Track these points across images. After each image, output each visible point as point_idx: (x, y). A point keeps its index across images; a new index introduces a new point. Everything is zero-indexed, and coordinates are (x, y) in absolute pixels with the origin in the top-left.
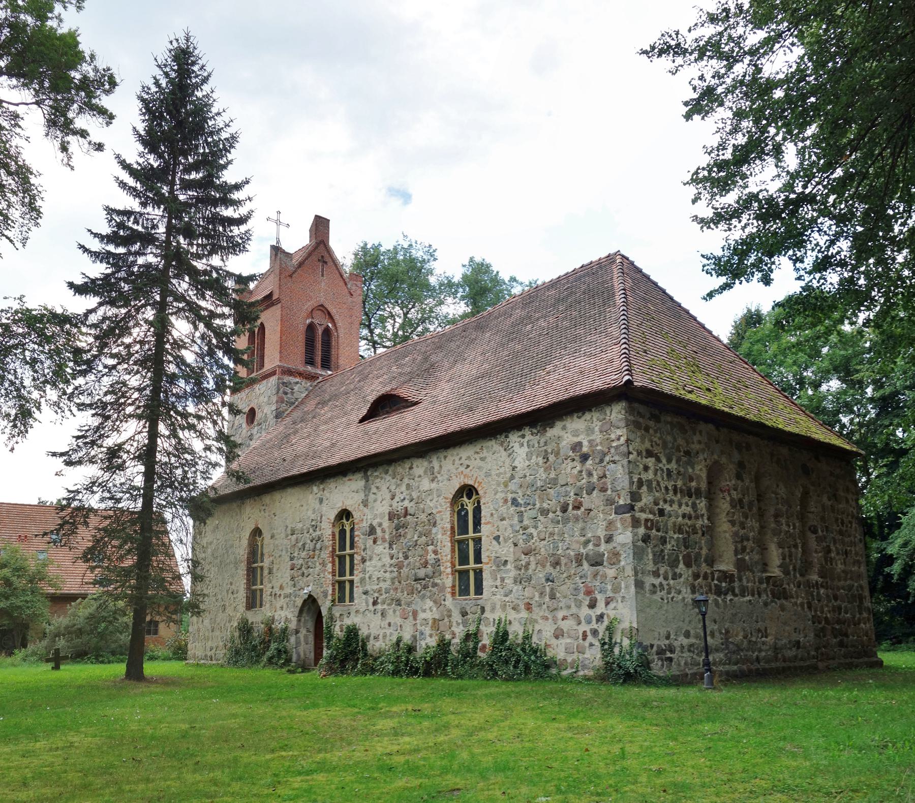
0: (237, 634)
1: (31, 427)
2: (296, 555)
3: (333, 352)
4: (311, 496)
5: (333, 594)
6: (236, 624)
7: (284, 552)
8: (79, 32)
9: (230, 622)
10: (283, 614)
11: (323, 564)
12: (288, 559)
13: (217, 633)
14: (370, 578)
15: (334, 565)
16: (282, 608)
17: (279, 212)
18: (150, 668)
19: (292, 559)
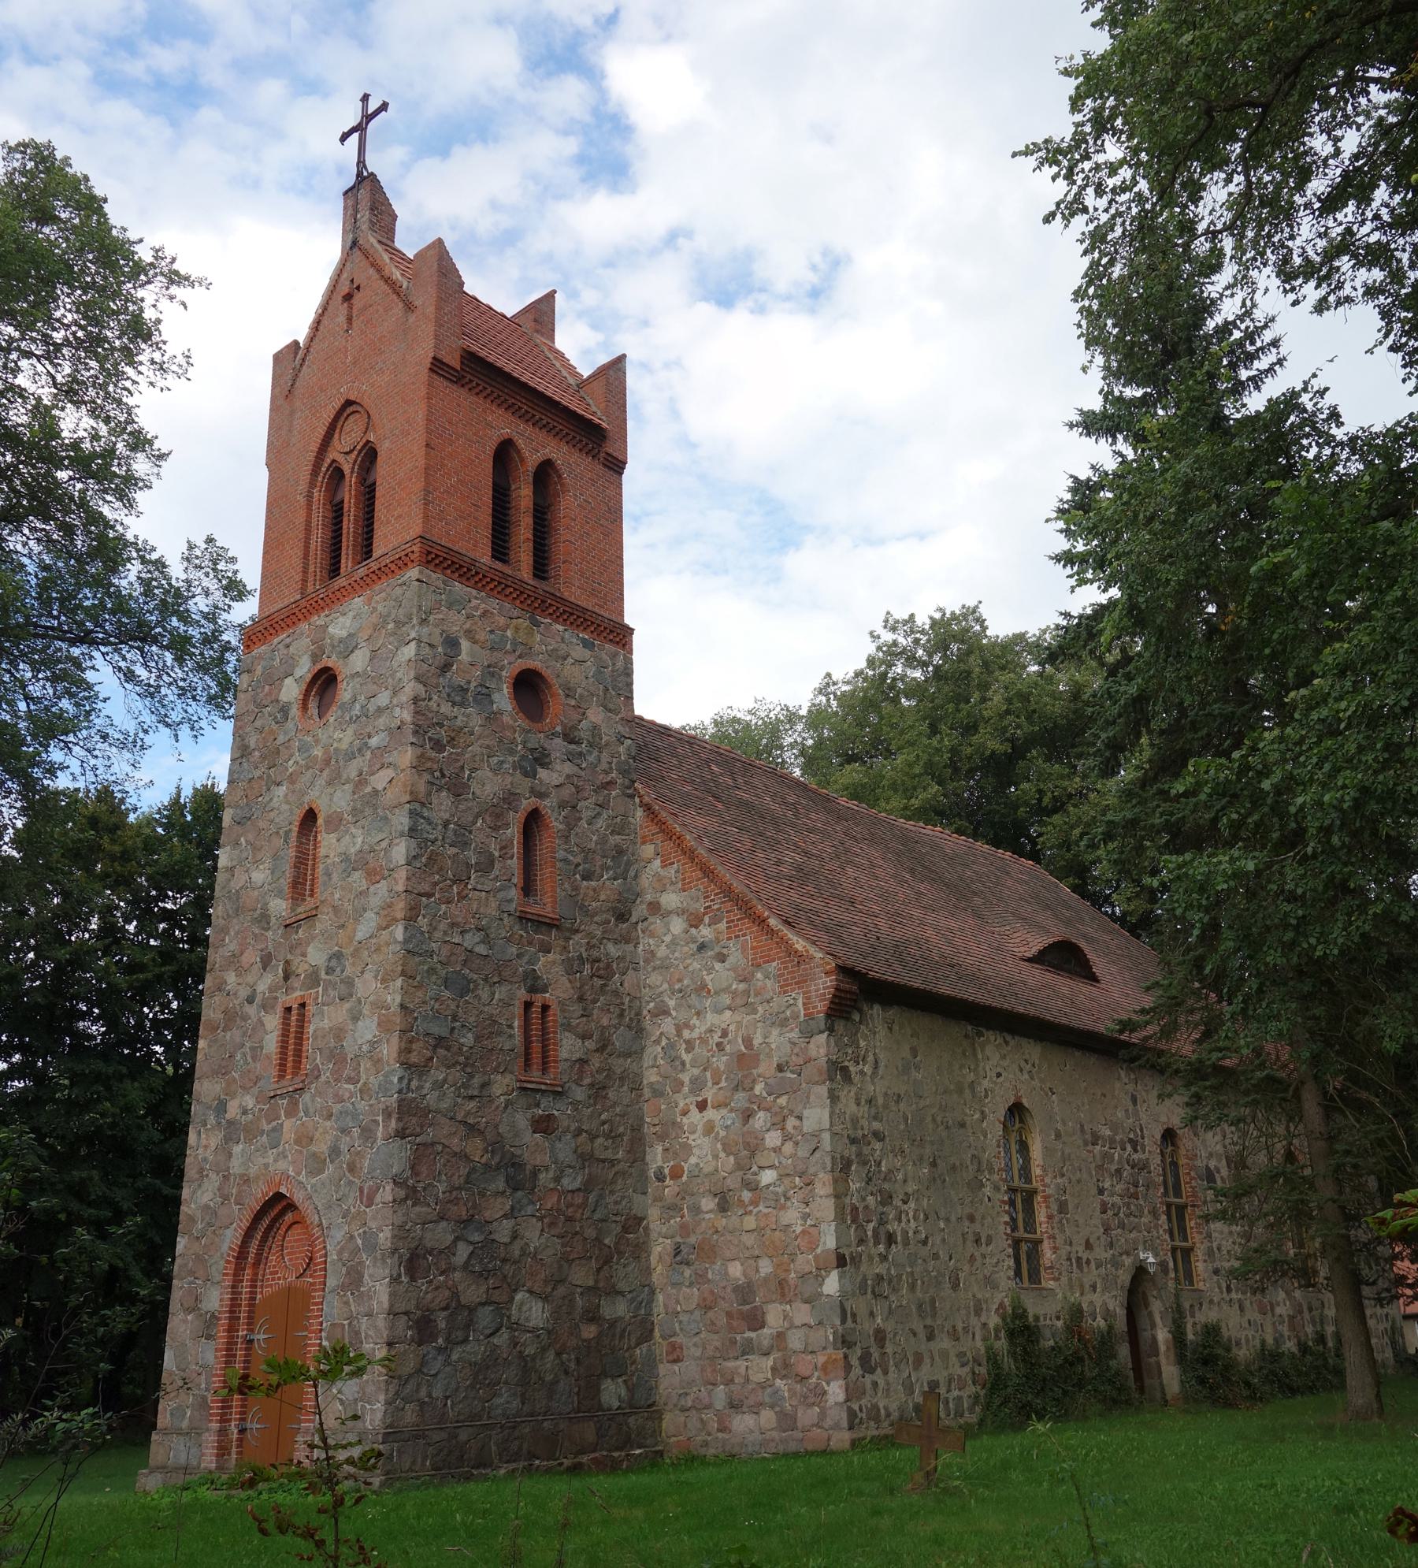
0: (1002, 1344)
1: (165, 343)
2: (1107, 1185)
3: (1092, 1060)
4: (1118, 1085)
5: (1176, 1270)
6: (994, 1320)
7: (1085, 1176)
8: (1076, 418)
9: (978, 1312)
10: (1097, 1299)
11: (1154, 1213)
12: (1094, 1191)
13: (944, 1343)
14: (1219, 1249)
15: (1169, 1219)
16: (1094, 1288)
17: (1370, 351)
18: (706, 1401)
19: (1101, 1192)
